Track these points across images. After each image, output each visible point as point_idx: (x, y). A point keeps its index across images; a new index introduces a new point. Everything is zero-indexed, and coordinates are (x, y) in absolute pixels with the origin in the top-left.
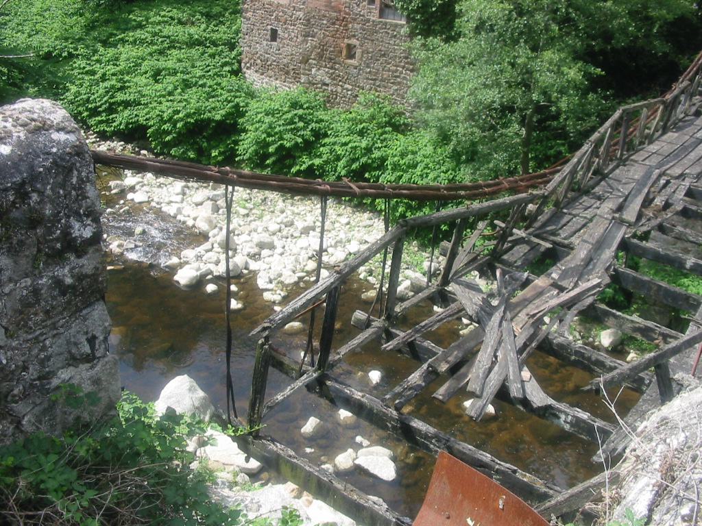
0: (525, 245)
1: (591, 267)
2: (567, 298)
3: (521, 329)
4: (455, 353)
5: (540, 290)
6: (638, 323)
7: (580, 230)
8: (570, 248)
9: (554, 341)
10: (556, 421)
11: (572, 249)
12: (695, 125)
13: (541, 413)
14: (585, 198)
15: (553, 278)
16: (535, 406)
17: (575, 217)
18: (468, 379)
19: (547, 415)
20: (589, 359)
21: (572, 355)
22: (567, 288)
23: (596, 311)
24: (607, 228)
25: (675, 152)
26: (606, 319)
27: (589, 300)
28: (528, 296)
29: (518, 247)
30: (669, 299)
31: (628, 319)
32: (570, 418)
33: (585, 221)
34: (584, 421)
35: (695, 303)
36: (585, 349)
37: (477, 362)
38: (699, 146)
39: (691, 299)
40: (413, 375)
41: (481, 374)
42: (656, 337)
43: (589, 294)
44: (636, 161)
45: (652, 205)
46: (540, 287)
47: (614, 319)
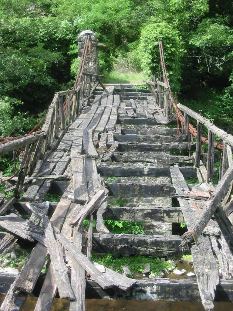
0: (34, 185)
1: (90, 185)
2: (90, 206)
3: (72, 236)
4: (32, 270)
5: (66, 208)
6: (146, 209)
7: (66, 169)
8: (67, 179)
9: (100, 239)
10: (143, 297)
11: (69, 180)
12: (92, 109)
13: (128, 295)
14: (55, 153)
15: (69, 199)
16: (125, 289)
17: (57, 163)
18: (55, 289)
19: (134, 294)
20: (133, 241)
21: (117, 245)
22: (86, 201)
23: (112, 212)
24: (84, 162)
25: (92, 121)
26: (121, 216)
27: (105, 206)
28: (60, 214)
29: (30, 188)
30: (149, 193)
31: (137, 210)
32: (155, 287)
33: (66, 164)
34: (168, 286)
35: (168, 190)
36: (127, 236)
37: (55, 272)
38: (102, 117)
39: (164, 187)
40: (3, 304)
41: (64, 280)
42: (162, 215)
43: (102, 201)
44: (73, 129)
45: (99, 148)
46: (65, 206)
47: (127, 214)
